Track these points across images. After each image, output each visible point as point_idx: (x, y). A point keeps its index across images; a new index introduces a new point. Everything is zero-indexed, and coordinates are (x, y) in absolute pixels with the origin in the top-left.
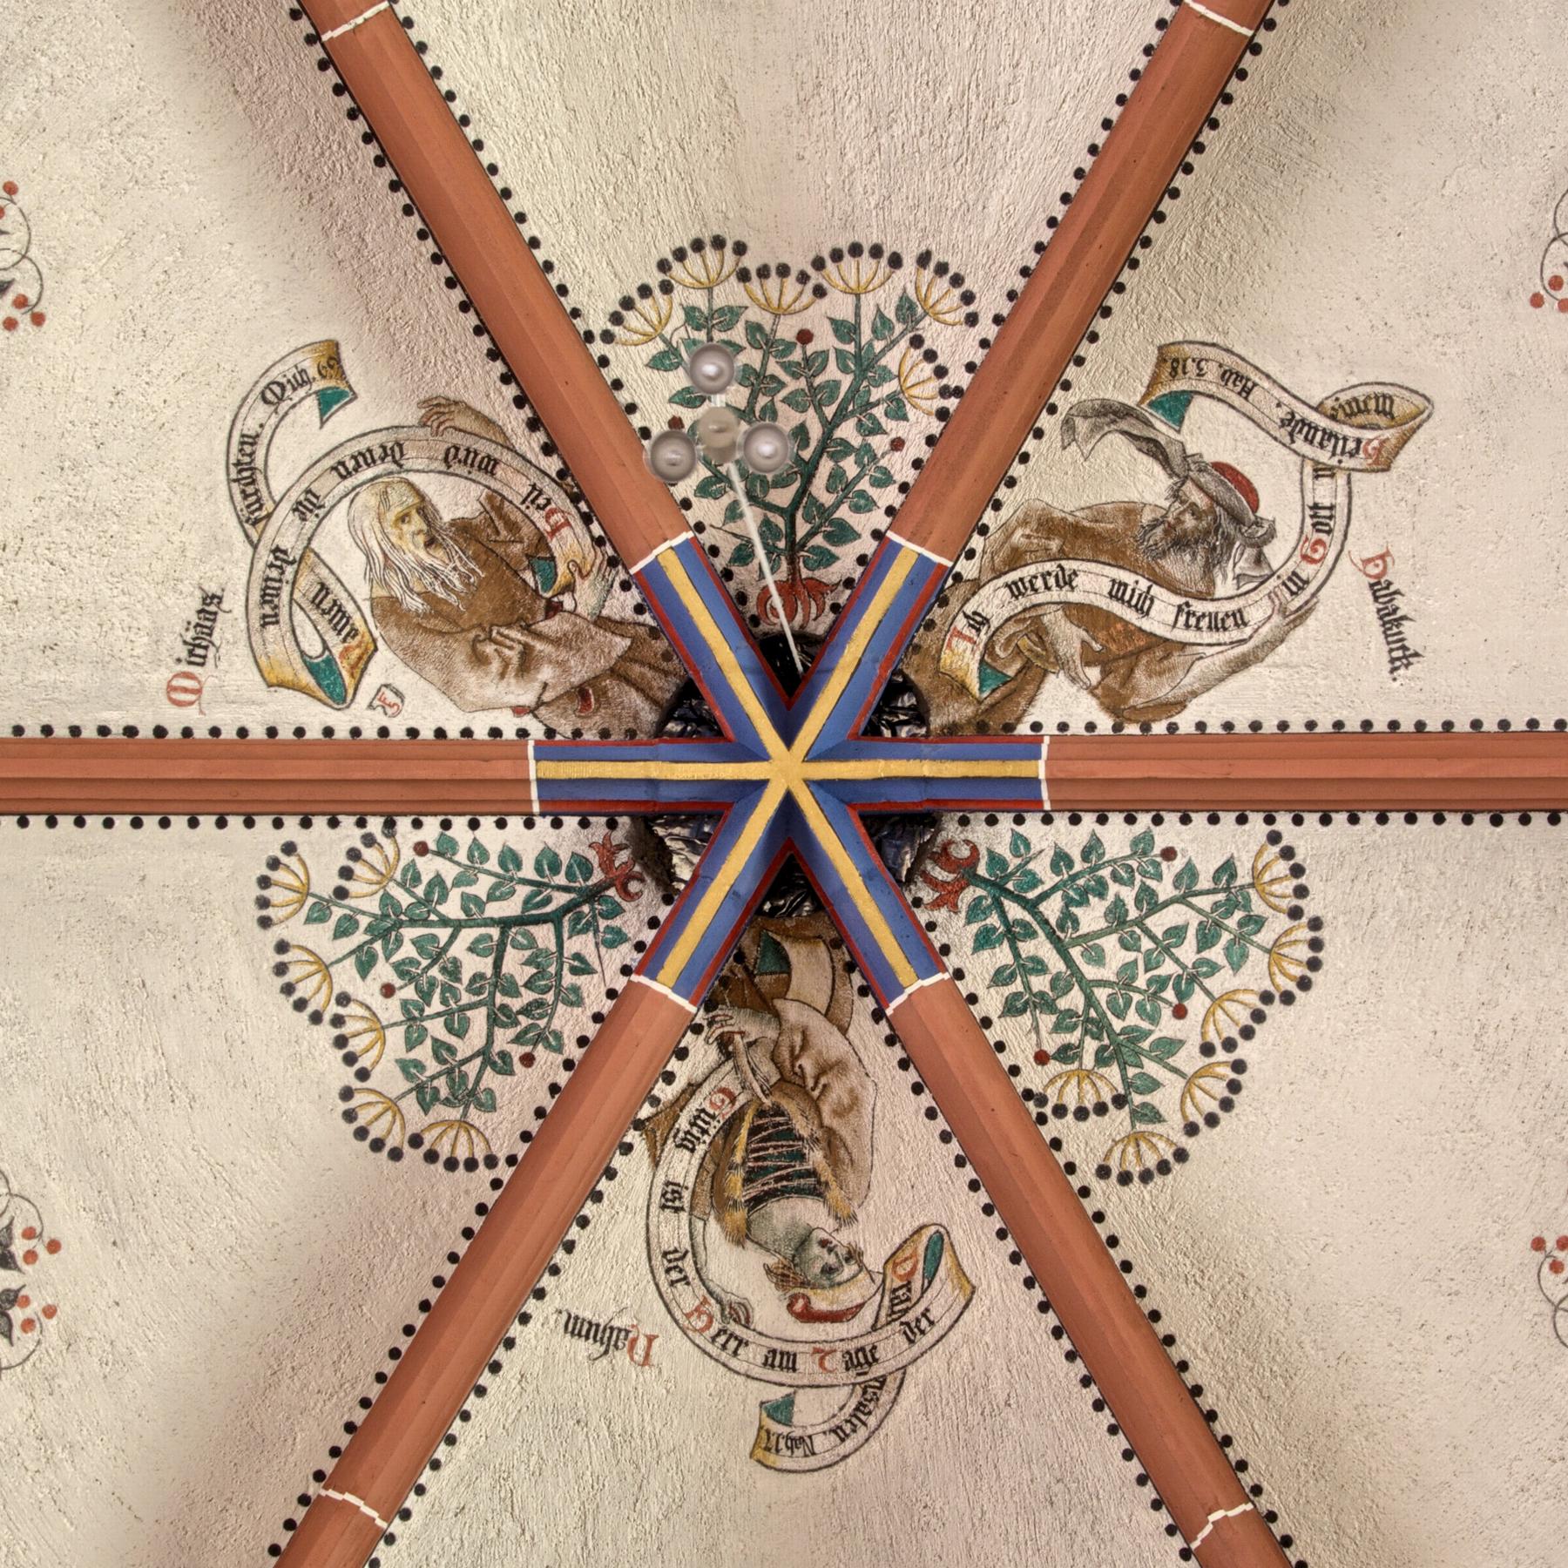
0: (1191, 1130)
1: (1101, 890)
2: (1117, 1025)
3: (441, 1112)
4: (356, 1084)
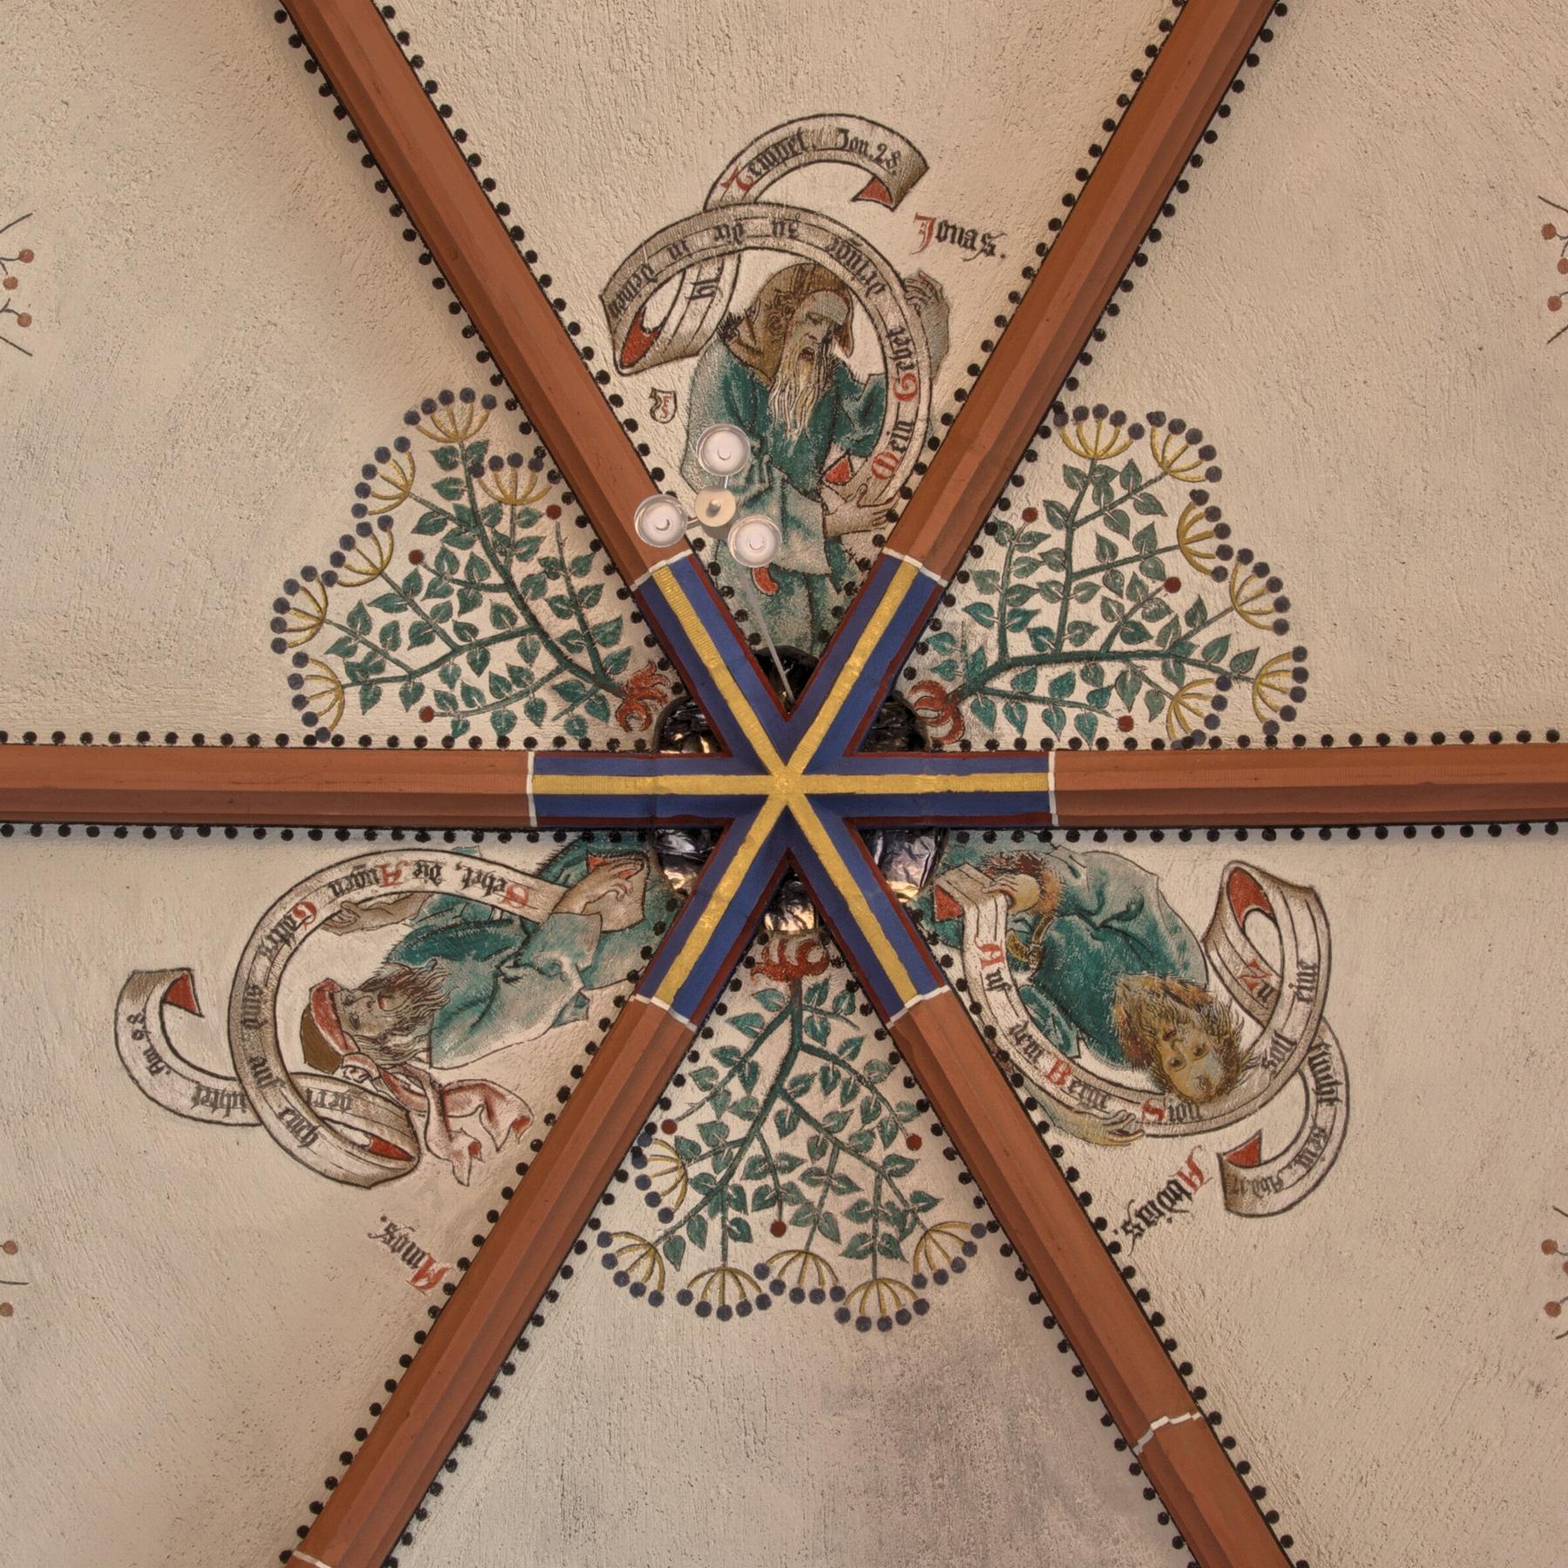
0: (403, 444)
1: (497, 683)
2: (478, 549)
3: (338, 665)
4: (1207, 486)
